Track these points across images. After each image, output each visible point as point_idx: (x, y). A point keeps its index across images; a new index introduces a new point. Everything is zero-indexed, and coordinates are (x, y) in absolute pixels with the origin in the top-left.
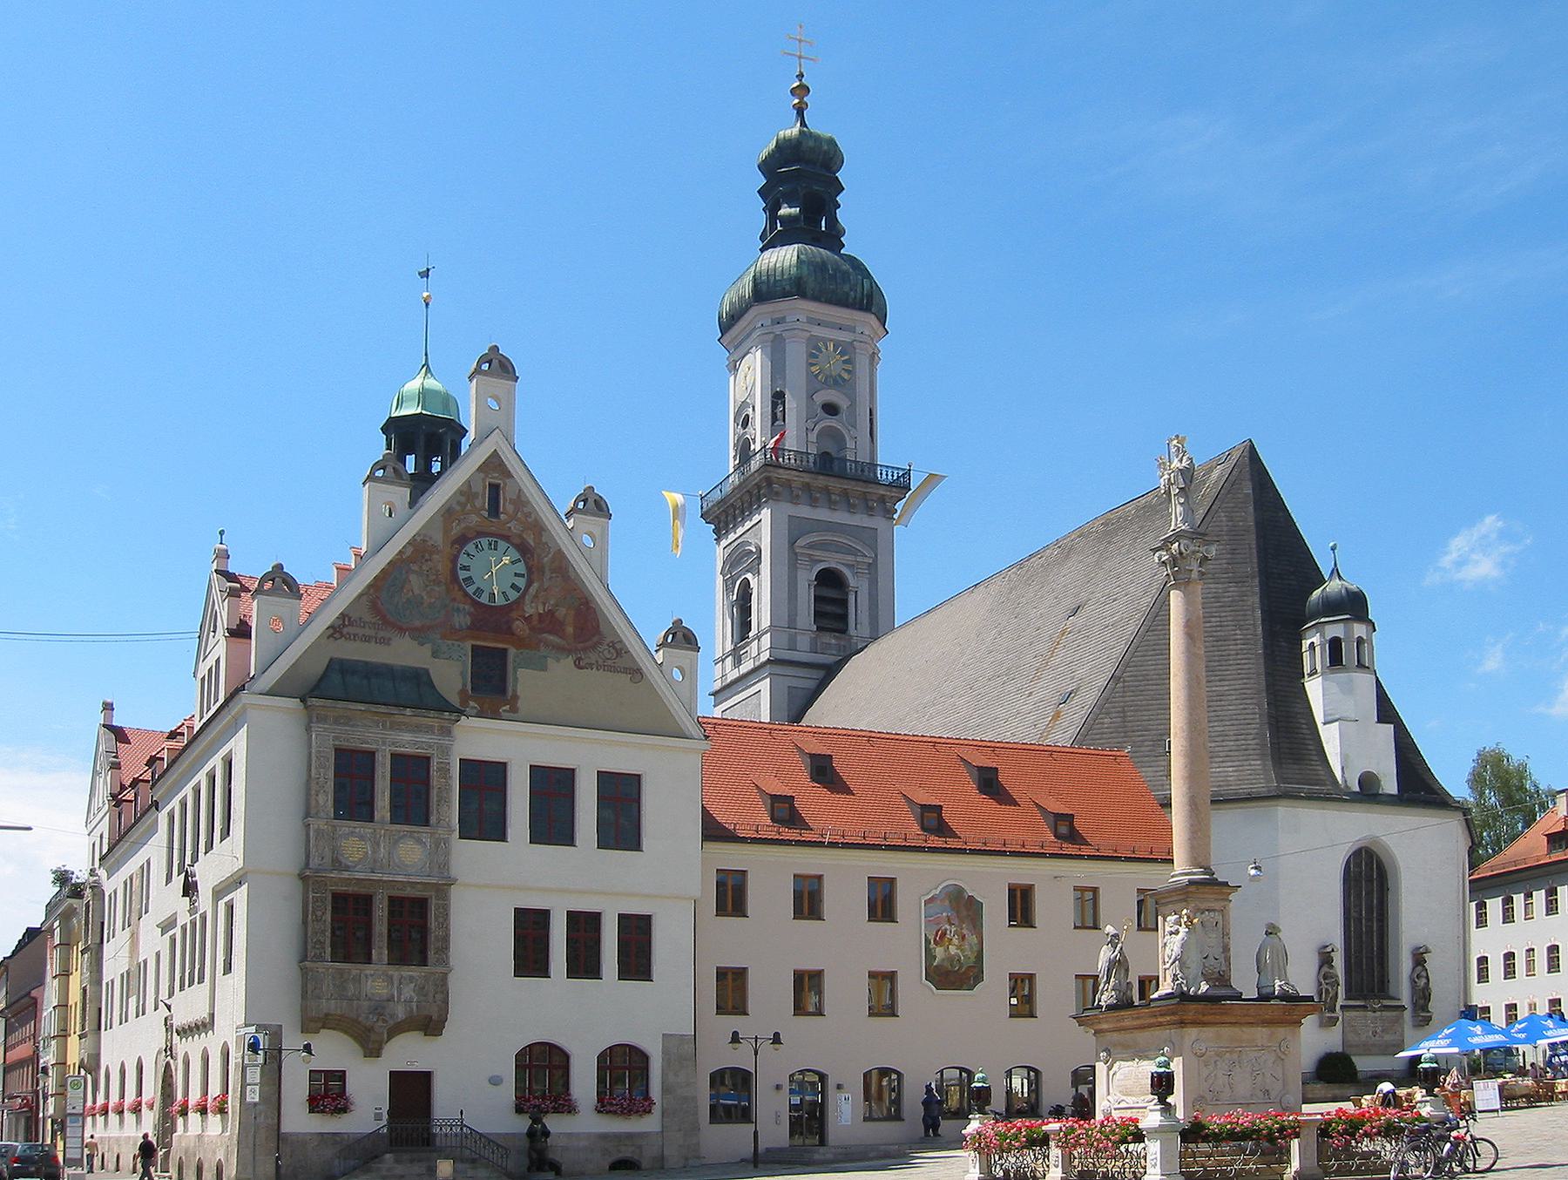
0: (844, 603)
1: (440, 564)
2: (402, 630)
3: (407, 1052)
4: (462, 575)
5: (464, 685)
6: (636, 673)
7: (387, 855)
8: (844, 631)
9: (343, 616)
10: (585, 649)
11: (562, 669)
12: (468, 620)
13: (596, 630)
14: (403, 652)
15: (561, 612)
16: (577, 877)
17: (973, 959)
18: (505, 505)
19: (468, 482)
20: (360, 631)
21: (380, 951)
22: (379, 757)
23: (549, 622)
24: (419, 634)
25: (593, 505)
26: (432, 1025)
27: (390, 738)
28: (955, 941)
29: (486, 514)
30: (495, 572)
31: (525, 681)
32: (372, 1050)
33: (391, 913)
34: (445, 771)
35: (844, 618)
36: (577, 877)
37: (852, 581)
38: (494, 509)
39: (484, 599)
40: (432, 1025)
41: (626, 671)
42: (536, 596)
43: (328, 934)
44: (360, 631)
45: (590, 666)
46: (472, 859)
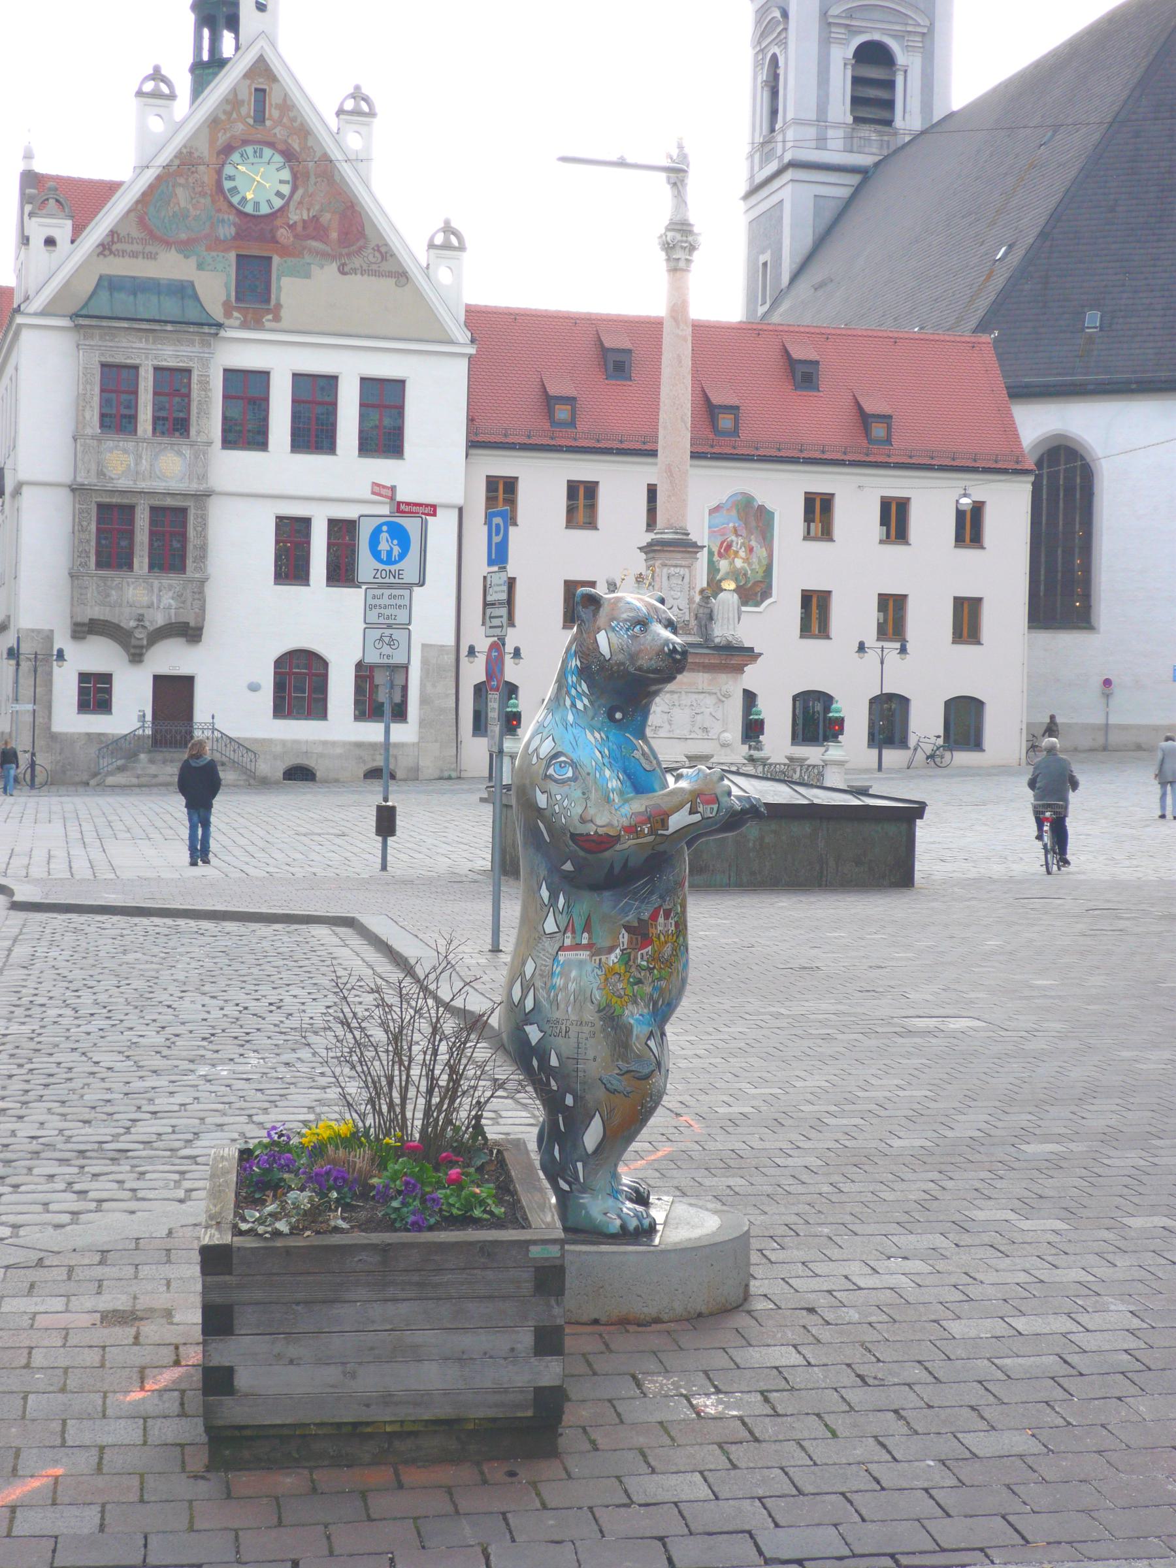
0: (890, 85)
1: (206, 175)
2: (168, 244)
3: (171, 658)
4: (227, 185)
5: (228, 295)
6: (402, 276)
7: (150, 468)
8: (889, 123)
9: (112, 233)
10: (348, 255)
11: (326, 275)
12: (233, 231)
13: (362, 234)
14: (169, 266)
15: (326, 218)
16: (340, 481)
17: (761, 574)
18: (273, 113)
19: (234, 91)
20: (129, 248)
21: (141, 561)
22: (142, 372)
23: (313, 229)
24: (185, 247)
25: (359, 108)
26: (189, 632)
27: (150, 355)
28: (742, 554)
29: (251, 121)
30: (260, 182)
31: (289, 289)
32: (136, 657)
33: (152, 522)
34: (205, 384)
35: (890, 105)
36: (340, 481)
37: (901, 58)
38: (260, 116)
39: (249, 209)
40: (190, 632)
41: (390, 274)
42: (300, 203)
43: (93, 543)
44: (129, 248)
45: (354, 271)
46: (234, 468)
